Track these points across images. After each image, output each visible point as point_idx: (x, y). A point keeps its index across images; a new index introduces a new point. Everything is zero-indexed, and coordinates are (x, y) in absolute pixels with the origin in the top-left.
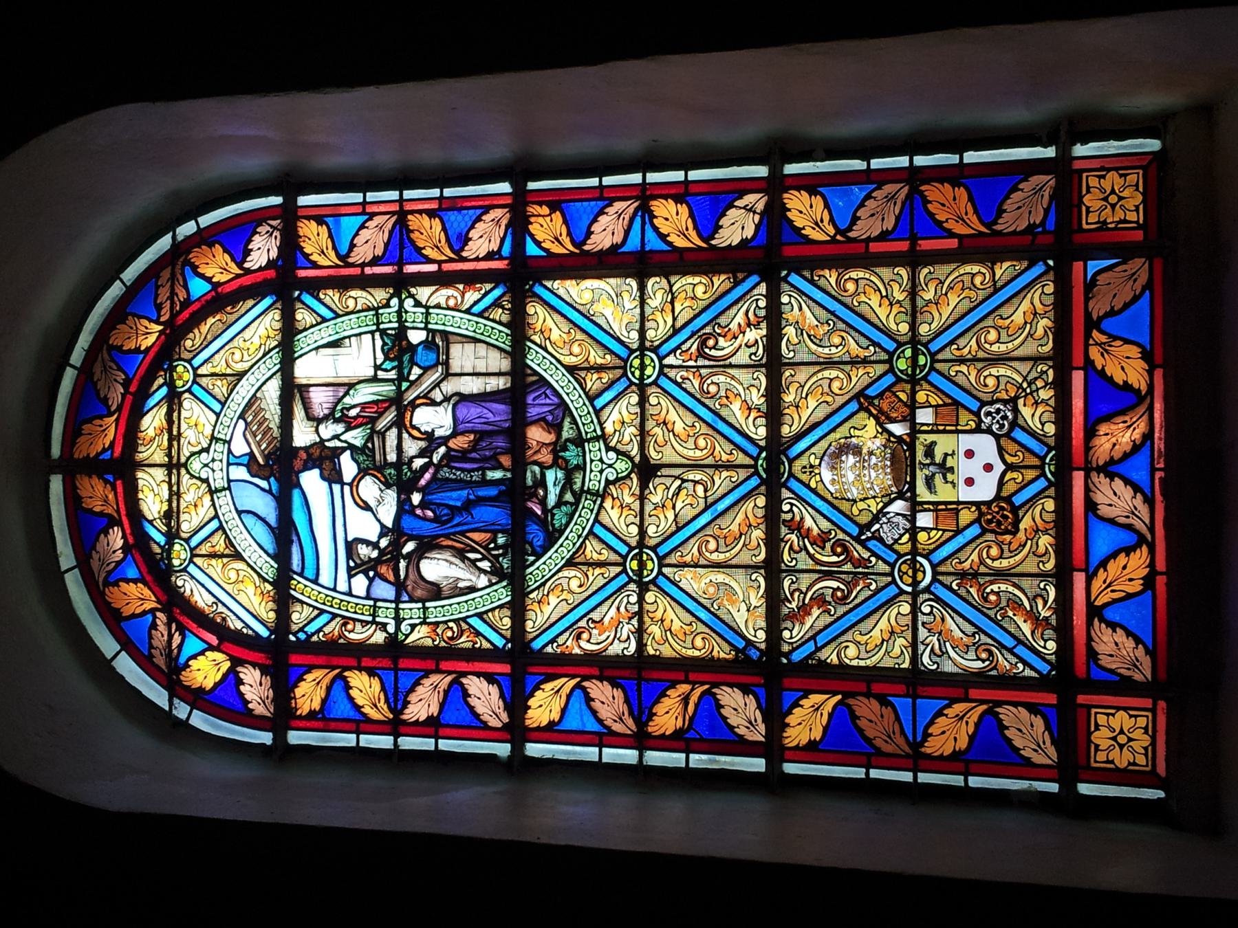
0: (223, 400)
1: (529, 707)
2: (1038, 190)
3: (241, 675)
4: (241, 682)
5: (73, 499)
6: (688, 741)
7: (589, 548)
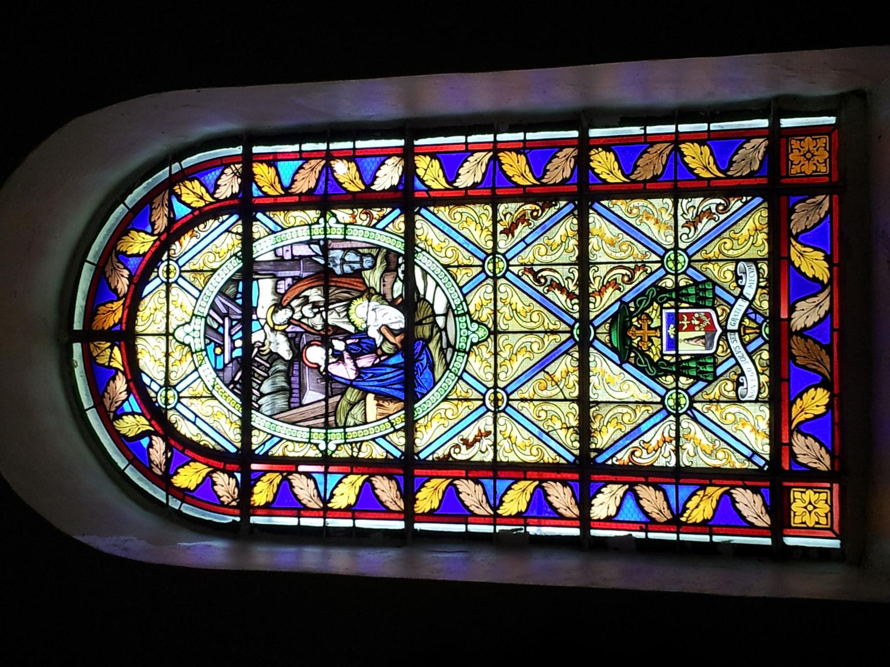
0: (200, 288)
1: (593, 505)
2: (756, 148)
3: (214, 479)
4: (214, 484)
5: (89, 359)
6: (711, 527)
7: (459, 389)
